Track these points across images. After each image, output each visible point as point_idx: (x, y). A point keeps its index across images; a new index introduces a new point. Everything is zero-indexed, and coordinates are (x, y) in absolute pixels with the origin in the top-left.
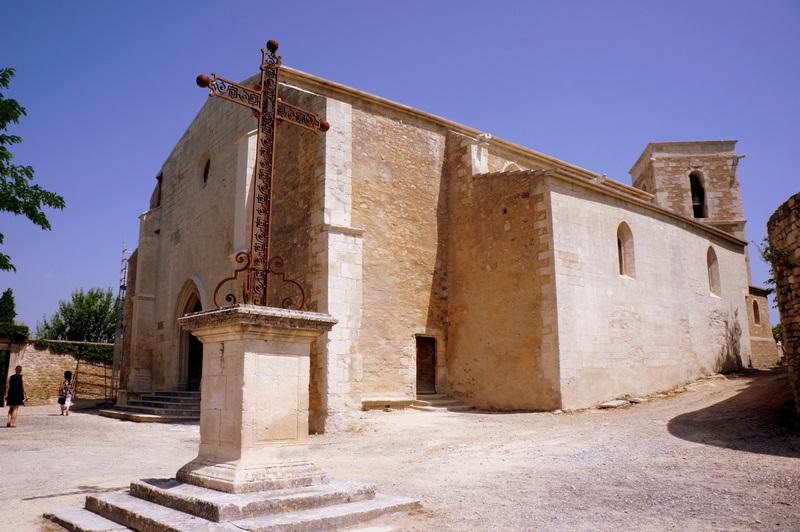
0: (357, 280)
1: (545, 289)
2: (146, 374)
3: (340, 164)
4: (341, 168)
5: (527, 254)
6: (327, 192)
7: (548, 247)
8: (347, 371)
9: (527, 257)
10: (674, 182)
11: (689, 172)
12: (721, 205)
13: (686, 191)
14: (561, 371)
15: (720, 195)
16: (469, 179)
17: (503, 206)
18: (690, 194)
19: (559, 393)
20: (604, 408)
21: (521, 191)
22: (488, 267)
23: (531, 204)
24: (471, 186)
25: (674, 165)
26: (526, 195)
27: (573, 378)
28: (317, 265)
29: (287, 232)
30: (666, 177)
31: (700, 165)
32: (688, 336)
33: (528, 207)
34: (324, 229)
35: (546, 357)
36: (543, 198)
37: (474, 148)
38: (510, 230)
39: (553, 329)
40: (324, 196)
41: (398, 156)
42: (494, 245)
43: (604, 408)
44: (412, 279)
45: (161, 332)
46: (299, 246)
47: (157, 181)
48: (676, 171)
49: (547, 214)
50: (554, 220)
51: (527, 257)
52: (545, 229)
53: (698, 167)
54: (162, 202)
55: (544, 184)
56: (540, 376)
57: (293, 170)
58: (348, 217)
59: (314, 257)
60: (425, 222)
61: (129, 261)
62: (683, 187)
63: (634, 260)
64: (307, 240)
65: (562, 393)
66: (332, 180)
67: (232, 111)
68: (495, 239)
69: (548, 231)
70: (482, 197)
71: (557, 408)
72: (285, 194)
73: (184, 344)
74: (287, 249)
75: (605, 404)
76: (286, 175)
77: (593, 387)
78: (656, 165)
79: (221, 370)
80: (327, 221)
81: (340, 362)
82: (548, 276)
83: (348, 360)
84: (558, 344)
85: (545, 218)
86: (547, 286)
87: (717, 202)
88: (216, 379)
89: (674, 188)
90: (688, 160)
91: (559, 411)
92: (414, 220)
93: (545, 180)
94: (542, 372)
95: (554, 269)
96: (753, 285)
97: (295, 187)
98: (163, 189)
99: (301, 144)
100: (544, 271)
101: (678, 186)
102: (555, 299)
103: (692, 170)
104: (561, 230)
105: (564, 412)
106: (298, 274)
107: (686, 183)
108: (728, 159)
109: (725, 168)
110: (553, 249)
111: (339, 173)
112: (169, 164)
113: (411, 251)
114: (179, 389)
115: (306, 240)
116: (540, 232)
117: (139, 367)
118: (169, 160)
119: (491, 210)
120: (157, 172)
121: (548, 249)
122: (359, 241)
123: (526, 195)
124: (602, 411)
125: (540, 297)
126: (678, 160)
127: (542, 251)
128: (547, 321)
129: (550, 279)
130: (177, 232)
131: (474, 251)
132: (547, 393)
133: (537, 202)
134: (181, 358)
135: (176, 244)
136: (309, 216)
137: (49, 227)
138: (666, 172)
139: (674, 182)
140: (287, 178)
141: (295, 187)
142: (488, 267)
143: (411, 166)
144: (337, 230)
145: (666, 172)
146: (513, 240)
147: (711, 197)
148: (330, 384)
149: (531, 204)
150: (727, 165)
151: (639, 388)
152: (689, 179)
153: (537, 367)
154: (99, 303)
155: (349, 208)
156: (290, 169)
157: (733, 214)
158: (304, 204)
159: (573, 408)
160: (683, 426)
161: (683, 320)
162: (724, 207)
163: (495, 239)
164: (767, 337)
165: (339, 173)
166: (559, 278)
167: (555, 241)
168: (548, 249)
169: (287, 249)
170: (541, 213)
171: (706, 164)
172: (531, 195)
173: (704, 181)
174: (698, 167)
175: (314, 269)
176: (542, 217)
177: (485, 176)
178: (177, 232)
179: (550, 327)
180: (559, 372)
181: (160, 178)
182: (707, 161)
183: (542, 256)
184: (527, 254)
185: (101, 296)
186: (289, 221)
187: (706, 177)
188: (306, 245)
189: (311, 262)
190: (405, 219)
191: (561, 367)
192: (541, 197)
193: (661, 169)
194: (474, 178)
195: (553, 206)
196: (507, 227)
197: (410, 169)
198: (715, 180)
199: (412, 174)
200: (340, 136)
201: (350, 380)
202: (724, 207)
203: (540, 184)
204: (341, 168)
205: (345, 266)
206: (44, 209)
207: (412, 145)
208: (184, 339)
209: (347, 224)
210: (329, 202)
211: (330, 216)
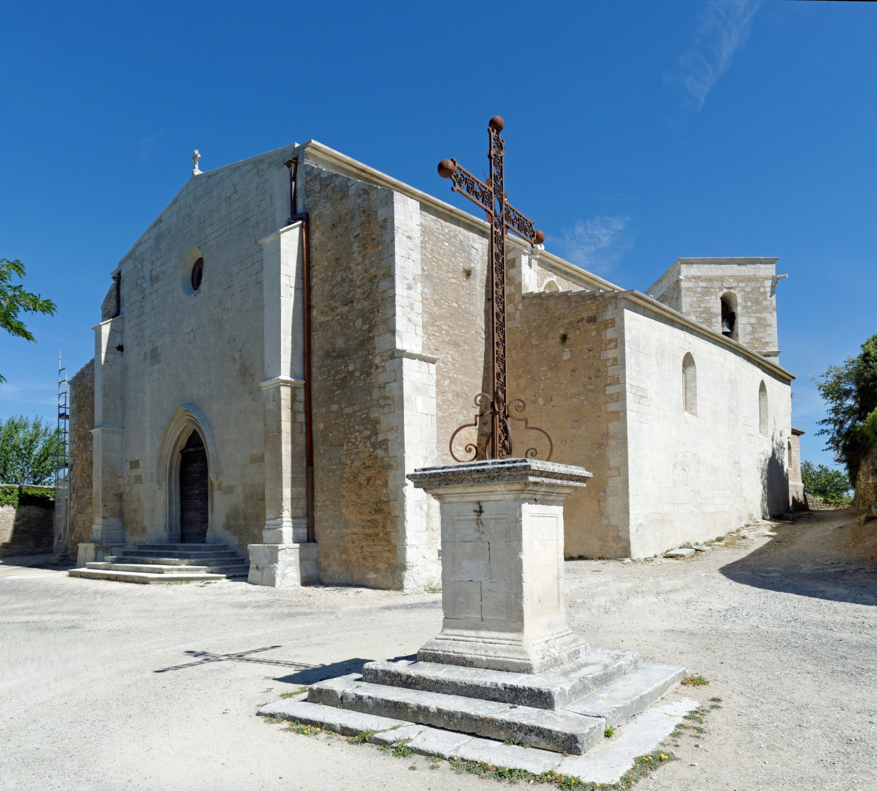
0: (433, 415)
1: (613, 427)
2: (114, 521)
3: (410, 277)
4: (411, 281)
5: (591, 387)
6: (398, 310)
7: (619, 380)
8: (424, 519)
9: (592, 391)
10: (703, 305)
11: (721, 294)
12: (753, 332)
13: (715, 316)
14: (631, 516)
15: (753, 321)
16: (517, 298)
17: (562, 332)
18: (720, 318)
19: (628, 541)
20: (672, 557)
21: (585, 315)
22: (541, 401)
23: (598, 331)
24: (520, 307)
25: (704, 284)
26: (592, 320)
27: (641, 525)
28: (386, 398)
29: (337, 357)
30: (695, 299)
31: (733, 285)
32: (739, 479)
33: (594, 333)
34: (397, 356)
35: (612, 502)
36: (618, 324)
37: (525, 259)
38: (570, 360)
39: (622, 471)
40: (394, 315)
41: (440, 267)
42: (549, 375)
43: (672, 557)
44: (455, 412)
45: (136, 472)
46: (357, 374)
47: (113, 282)
48: (706, 292)
49: (619, 342)
50: (627, 350)
51: (592, 391)
52: (615, 359)
53: (731, 288)
54: (122, 309)
55: (617, 307)
56: (605, 522)
57: (343, 280)
58: (419, 341)
59: (382, 387)
60: (467, 348)
61: (70, 383)
62: (712, 310)
63: (696, 395)
64: (371, 367)
65: (631, 540)
66: (402, 296)
67: (234, 197)
68: (551, 369)
69: (620, 362)
70: (535, 320)
71: (626, 557)
72: (333, 310)
73: (173, 487)
74: (339, 377)
75: (672, 553)
76: (334, 287)
77: (658, 534)
78: (684, 285)
79: (477, 535)
80: (399, 346)
81: (418, 510)
82: (617, 413)
83: (425, 507)
84: (628, 487)
85: (616, 346)
86: (616, 423)
87: (749, 329)
88: (468, 545)
89: (702, 312)
90: (721, 279)
91: (627, 560)
92: (456, 345)
93: (619, 302)
94: (607, 517)
95: (625, 405)
96: (794, 428)
97: (349, 302)
98: (122, 293)
99: (355, 248)
100: (613, 407)
101: (707, 310)
102: (626, 437)
103: (725, 291)
104: (633, 360)
105: (634, 561)
106: (357, 407)
107: (717, 308)
108: (766, 279)
109: (762, 290)
110: (625, 383)
111: (409, 288)
112: (131, 261)
113: (454, 381)
114: (170, 540)
115: (368, 369)
116: (609, 364)
117: (106, 515)
118: (131, 255)
119: (546, 336)
120: (114, 268)
121: (618, 383)
122: (433, 367)
123: (592, 320)
124: (670, 560)
125: (606, 436)
126: (710, 280)
127: (611, 384)
128: (614, 462)
129: (620, 416)
130: (154, 350)
131: (523, 382)
132: (614, 541)
133: (606, 328)
134: (170, 504)
135: (153, 365)
136: (373, 338)
137: (32, 339)
138: (695, 292)
139: (703, 305)
140: (335, 291)
141: (349, 302)
142: (541, 401)
143: (453, 281)
144: (412, 356)
145: (695, 292)
146: (574, 371)
147: (742, 322)
148: (409, 533)
149: (598, 331)
150: (764, 287)
151: (700, 537)
152: (720, 301)
153: (601, 513)
154: (21, 434)
155: (420, 330)
156: (339, 279)
157: (767, 343)
158: (364, 323)
159: (642, 557)
160: (732, 572)
161: (736, 463)
162: (756, 335)
163: (551, 369)
164: (797, 481)
165: (409, 288)
166: (630, 415)
167: (628, 373)
168: (618, 383)
169: (339, 377)
170: (611, 341)
171: (741, 285)
172: (599, 319)
173: (737, 305)
174: (731, 288)
175: (382, 402)
176: (612, 345)
177: (539, 296)
178: (154, 350)
179: (618, 469)
180: (629, 519)
181: (118, 278)
182: (742, 281)
183: (610, 390)
184: (591, 387)
185: (25, 426)
186: (340, 343)
187: (739, 300)
188: (368, 374)
189: (376, 394)
190: (448, 343)
191: (631, 512)
192: (612, 322)
193: (689, 289)
194: (523, 298)
195: (626, 334)
196: (566, 356)
197: (451, 284)
198: (749, 304)
199: (454, 290)
200: (408, 242)
201: (427, 529)
202: (756, 335)
203: (610, 308)
204: (411, 281)
205: (419, 400)
206: (22, 316)
207: (454, 255)
208: (173, 481)
209: (417, 350)
210: (400, 323)
211: (401, 340)
